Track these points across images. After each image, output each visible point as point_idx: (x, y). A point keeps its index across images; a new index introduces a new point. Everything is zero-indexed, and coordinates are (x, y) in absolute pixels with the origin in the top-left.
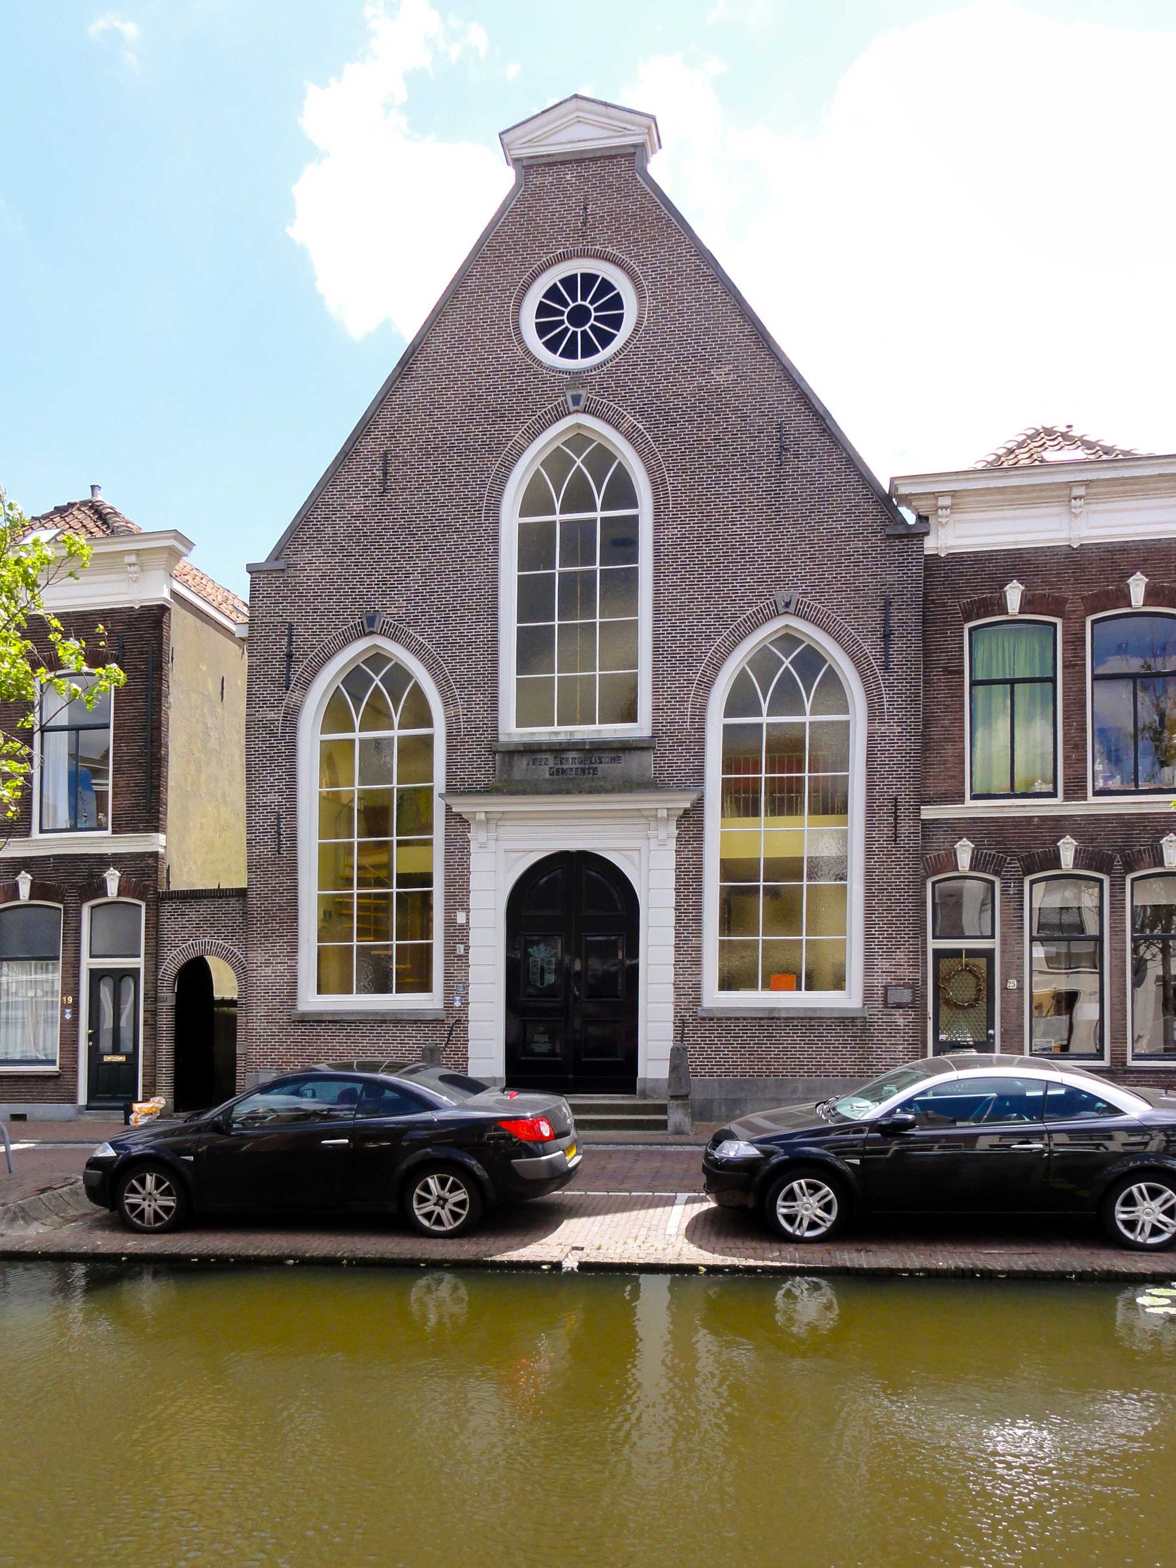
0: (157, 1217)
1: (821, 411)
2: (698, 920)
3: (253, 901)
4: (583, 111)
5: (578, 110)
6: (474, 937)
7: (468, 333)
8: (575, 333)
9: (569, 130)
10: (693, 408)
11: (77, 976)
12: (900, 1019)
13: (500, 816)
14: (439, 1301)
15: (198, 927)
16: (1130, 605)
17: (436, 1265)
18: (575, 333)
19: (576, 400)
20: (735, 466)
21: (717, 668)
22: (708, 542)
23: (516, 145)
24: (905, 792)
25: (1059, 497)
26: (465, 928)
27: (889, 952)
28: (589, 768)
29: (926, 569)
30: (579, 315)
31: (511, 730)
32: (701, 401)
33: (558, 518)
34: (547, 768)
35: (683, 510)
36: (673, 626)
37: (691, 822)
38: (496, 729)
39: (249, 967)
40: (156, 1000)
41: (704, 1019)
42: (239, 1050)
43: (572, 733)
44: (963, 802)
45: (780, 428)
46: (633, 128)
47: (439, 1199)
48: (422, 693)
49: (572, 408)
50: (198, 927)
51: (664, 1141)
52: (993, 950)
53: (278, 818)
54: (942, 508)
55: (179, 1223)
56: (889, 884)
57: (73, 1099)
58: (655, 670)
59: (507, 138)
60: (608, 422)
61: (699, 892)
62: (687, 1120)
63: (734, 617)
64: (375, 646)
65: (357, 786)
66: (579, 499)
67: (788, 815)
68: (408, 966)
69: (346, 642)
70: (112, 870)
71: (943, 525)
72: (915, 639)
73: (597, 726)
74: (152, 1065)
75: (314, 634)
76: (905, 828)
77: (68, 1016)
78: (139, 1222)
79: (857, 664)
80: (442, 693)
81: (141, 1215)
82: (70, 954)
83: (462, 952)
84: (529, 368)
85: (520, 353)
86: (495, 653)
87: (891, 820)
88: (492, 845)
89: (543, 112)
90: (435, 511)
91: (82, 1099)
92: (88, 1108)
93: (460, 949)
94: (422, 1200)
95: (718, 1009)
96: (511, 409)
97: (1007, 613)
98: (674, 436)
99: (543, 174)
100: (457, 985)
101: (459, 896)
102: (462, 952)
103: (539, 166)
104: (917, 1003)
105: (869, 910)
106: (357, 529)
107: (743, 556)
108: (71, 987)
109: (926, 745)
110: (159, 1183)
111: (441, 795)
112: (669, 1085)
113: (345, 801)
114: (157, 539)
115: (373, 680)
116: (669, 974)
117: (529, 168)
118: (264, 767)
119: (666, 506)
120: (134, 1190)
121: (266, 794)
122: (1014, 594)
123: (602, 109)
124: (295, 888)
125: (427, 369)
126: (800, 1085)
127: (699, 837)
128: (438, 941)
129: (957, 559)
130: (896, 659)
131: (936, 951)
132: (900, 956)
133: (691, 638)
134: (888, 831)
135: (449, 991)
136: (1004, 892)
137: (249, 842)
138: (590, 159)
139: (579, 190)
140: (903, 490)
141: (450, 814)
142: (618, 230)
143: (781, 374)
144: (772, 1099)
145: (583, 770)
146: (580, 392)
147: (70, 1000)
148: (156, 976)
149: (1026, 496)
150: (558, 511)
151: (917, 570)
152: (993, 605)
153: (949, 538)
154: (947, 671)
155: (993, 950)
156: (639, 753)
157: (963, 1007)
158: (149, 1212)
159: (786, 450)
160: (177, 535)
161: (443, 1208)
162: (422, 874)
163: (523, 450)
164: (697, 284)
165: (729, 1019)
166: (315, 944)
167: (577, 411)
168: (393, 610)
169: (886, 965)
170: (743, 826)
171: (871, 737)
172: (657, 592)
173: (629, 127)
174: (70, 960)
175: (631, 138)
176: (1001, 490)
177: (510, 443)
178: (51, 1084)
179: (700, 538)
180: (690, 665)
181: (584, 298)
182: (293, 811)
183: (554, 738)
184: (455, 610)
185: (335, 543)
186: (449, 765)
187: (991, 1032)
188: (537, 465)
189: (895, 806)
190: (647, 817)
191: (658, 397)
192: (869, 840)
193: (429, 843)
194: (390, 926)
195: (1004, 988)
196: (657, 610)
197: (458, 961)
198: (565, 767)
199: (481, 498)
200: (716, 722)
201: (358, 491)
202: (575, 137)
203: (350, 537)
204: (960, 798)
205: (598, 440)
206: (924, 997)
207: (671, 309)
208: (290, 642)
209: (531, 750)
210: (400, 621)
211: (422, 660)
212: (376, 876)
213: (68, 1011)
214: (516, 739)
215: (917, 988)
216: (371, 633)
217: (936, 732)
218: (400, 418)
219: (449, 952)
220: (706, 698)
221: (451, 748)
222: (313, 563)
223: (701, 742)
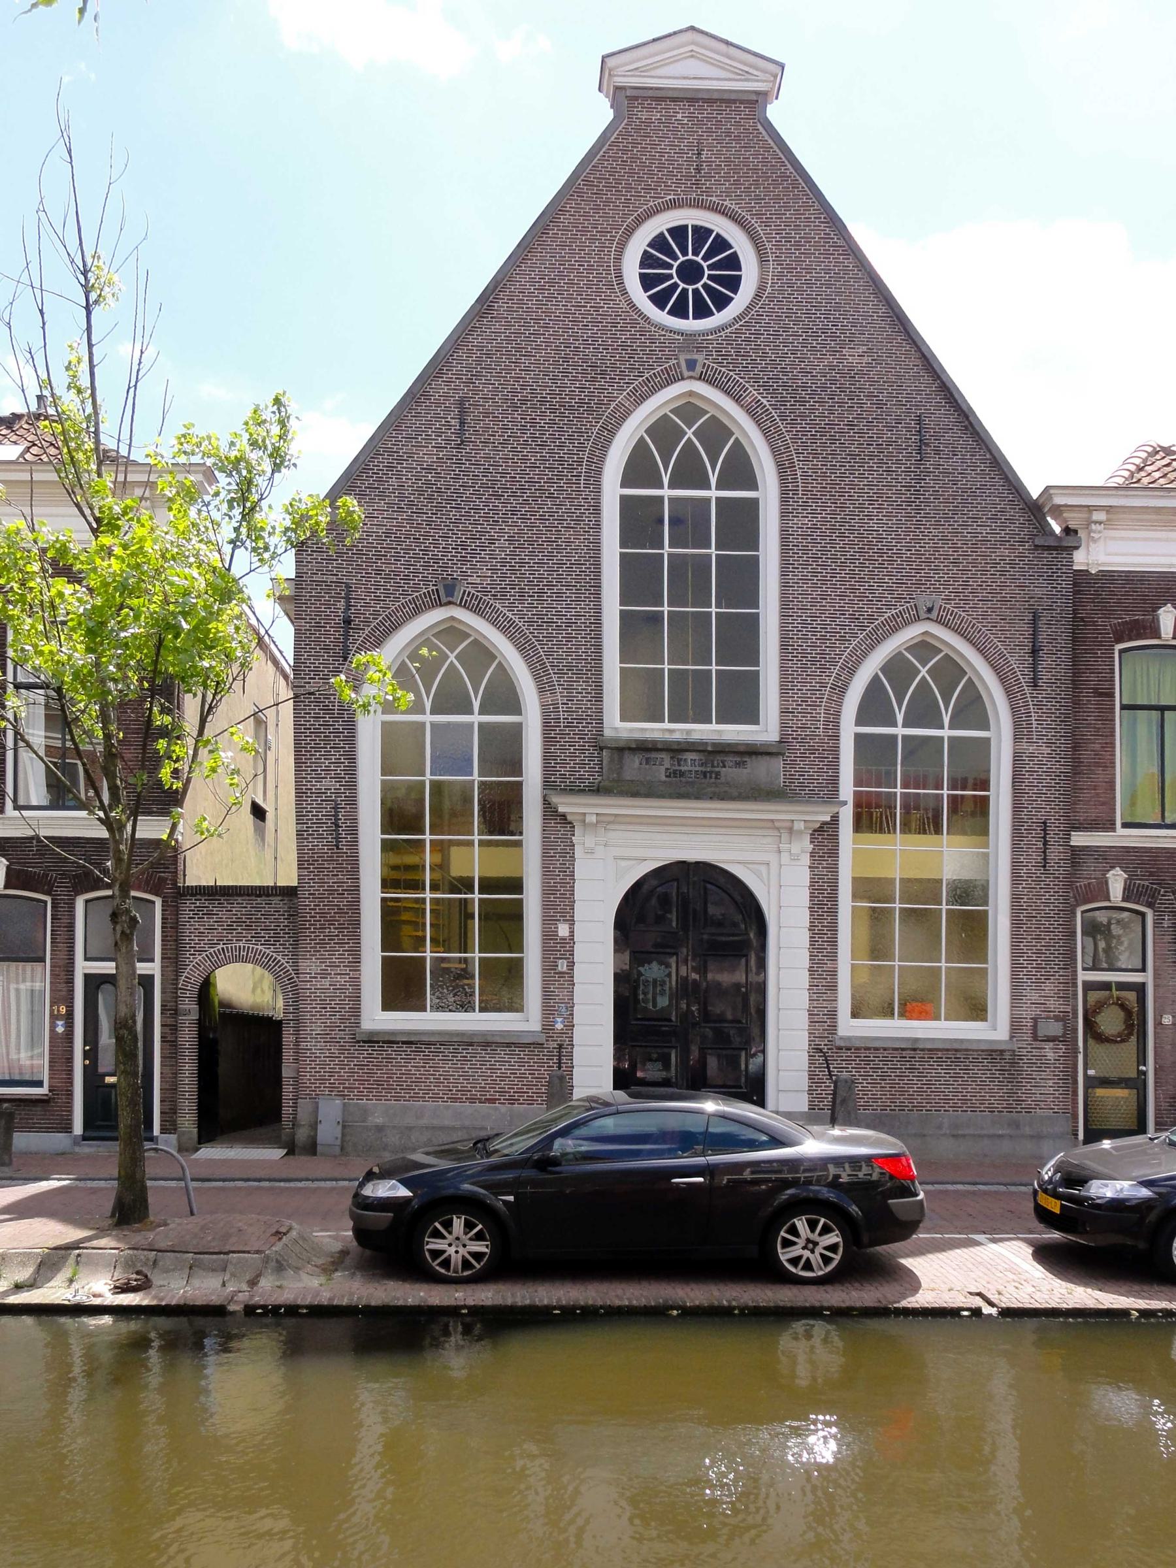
0: (466, 1264)
2: (834, 942)
3: (306, 901)
4: (697, 44)
5: (693, 43)
6: (580, 952)
9: (676, 64)
11: (70, 981)
14: (809, 1352)
16: (1159, 637)
17: (813, 1313)
19: (691, 365)
20: (871, 456)
22: (842, 536)
23: (620, 71)
24: (1054, 815)
27: (1038, 982)
28: (711, 772)
29: (1075, 584)
30: (692, 273)
31: (617, 725)
34: (663, 769)
35: (815, 499)
36: (804, 622)
37: (825, 835)
40: (176, 1012)
41: (840, 1048)
42: (287, 1072)
43: (688, 732)
44: (1114, 829)
45: (919, 420)
46: (756, 73)
47: (809, 1244)
49: (686, 374)
50: (230, 929)
54: (1096, 522)
55: (495, 1270)
57: (67, 1128)
58: (783, 669)
61: (833, 912)
63: (871, 619)
64: (452, 618)
69: (418, 611)
71: (1095, 541)
72: (1065, 655)
74: (171, 1091)
75: (377, 599)
76: (1056, 853)
77: (60, 1030)
78: (443, 1271)
79: (1003, 680)
80: (537, 678)
81: (446, 1263)
82: (63, 955)
83: (565, 969)
84: (634, 323)
85: (623, 304)
86: (599, 637)
89: (654, 40)
90: (523, 473)
91: (78, 1128)
92: (84, 1138)
93: (562, 966)
94: (787, 1244)
98: (803, 416)
99: (650, 109)
101: (560, 902)
102: (565, 969)
103: (645, 98)
104: (1068, 1038)
106: (428, 483)
108: (63, 995)
109: (1076, 769)
110: (469, 1226)
117: (630, 101)
118: (317, 748)
120: (437, 1234)
121: (319, 779)
123: (723, 47)
124: (356, 889)
125: (510, 310)
126: (945, 1120)
127: (834, 853)
129: (1108, 577)
130: (1045, 677)
131: (1085, 983)
132: (1049, 987)
133: (823, 638)
134: (1037, 857)
135: (548, 1010)
136: (1157, 924)
137: (299, 834)
138: (705, 100)
140: (1058, 500)
141: (550, 811)
142: (737, 183)
143: (918, 362)
144: (915, 1135)
145: (705, 774)
146: (695, 357)
147: (63, 1010)
148: (177, 984)
151: (1066, 585)
152: (1145, 628)
154: (1098, 693)
156: (768, 758)
157: (1116, 1042)
158: (456, 1260)
159: (927, 445)
161: (812, 1252)
162: (509, 879)
163: (628, 413)
164: (827, 254)
165: (869, 1049)
167: (691, 377)
168: (476, 578)
169: (1035, 996)
170: (874, 842)
171: (1017, 758)
173: (751, 71)
174: (61, 963)
175: (756, 84)
176: (1158, 510)
177: (613, 405)
178: (38, 1109)
180: (823, 668)
181: (705, 259)
182: (353, 801)
183: (667, 736)
184: (550, 585)
187: (1142, 1068)
188: (642, 432)
189: (1045, 830)
190: (778, 829)
191: (785, 373)
192: (1016, 865)
194: (462, 935)
195: (1158, 1024)
196: (785, 604)
197: (559, 977)
198: (683, 769)
199: (580, 463)
200: (849, 729)
201: (428, 439)
202: (692, 73)
204: (1110, 826)
205: (712, 411)
206: (1075, 1030)
207: (799, 276)
208: (348, 606)
209: (645, 748)
211: (511, 638)
213: (60, 1023)
214: (624, 735)
215: (1066, 1019)
216: (450, 603)
217: (1086, 755)
218: (479, 361)
221: (548, 740)
223: (835, 750)
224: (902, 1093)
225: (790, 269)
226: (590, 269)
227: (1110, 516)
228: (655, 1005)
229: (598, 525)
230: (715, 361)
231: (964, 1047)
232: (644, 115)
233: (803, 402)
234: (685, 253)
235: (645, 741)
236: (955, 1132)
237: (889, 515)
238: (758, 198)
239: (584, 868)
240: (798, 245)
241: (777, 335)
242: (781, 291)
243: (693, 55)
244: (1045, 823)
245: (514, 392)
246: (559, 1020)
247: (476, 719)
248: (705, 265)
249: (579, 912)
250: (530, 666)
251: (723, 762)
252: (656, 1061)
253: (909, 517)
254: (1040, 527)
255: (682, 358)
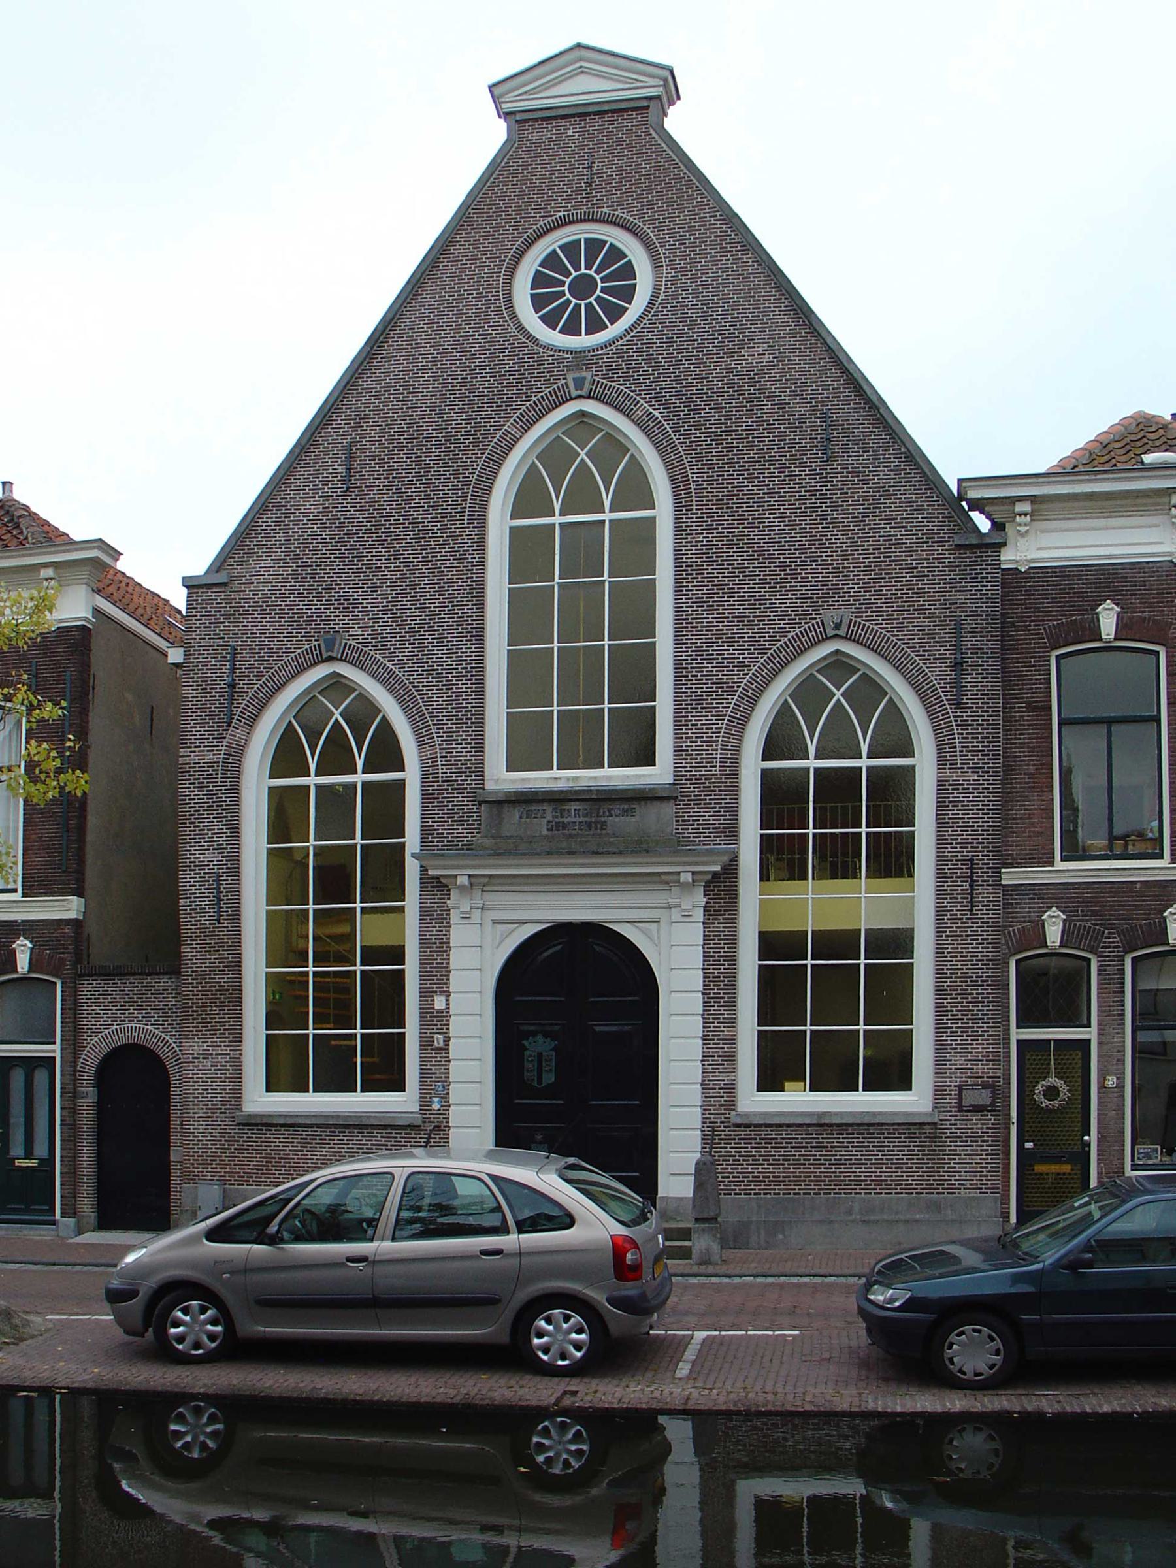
1: (874, 399)
2: (732, 1006)
5: (581, 60)
7: (450, 307)
8: (578, 306)
10: (720, 393)
12: (976, 1123)
13: (486, 880)
15: (123, 1009)
18: (578, 306)
20: (772, 462)
21: (753, 702)
22: (740, 551)
25: (1158, 504)
26: (445, 1014)
28: (596, 823)
31: (500, 777)
32: (731, 385)
33: (557, 519)
34: (544, 821)
35: (710, 513)
37: (721, 888)
38: (481, 774)
39: (183, 1058)
43: (576, 778)
48: (570, 923)
51: (687, 1271)
52: (1089, 1041)
53: (218, 880)
56: (964, 962)
58: (677, 702)
59: (497, 92)
60: (617, 409)
61: (732, 973)
62: (715, 1247)
63: (773, 640)
65: (312, 842)
66: (583, 496)
67: (843, 878)
68: (376, 1059)
70: (22, 941)
71: (1023, 535)
73: (606, 771)
75: (262, 660)
76: (984, 895)
80: (416, 731)
84: (523, 346)
85: (512, 329)
86: (481, 682)
87: (967, 885)
88: (476, 916)
93: (439, 1040)
95: (755, 1114)
96: (501, 394)
97: (1101, 640)
98: (697, 426)
100: (435, 1084)
101: (436, 975)
102: (442, 1044)
103: (536, 120)
105: (940, 993)
106: (314, 535)
107: (783, 567)
109: (1007, 796)
111: (413, 855)
112: (694, 1206)
113: (298, 857)
114: (82, 549)
115: (333, 714)
116: (695, 1071)
118: (201, 819)
119: (689, 507)
122: (1108, 619)
127: (732, 907)
128: (412, 1030)
129: (1040, 574)
130: (970, 691)
132: (978, 1049)
133: (720, 666)
135: (426, 1091)
139: (582, 147)
140: (972, 494)
144: (821, 1222)
145: (589, 825)
146: (584, 374)
148: (75, 1067)
149: (1118, 502)
150: (557, 512)
151: (992, 587)
153: (1033, 548)
154: (1030, 707)
155: (1089, 1041)
156: (657, 804)
160: (100, 544)
164: (724, 253)
166: (263, 1032)
170: (788, 892)
171: (941, 785)
172: (678, 610)
175: (644, 90)
176: (1091, 496)
177: (500, 433)
179: (730, 544)
180: (720, 698)
181: (569, 302)
182: (235, 873)
184: (432, 630)
185: (287, 552)
186: (423, 818)
187: (1086, 1138)
190: (667, 883)
192: (940, 909)
193: (401, 910)
195: (1102, 1087)
197: (436, 1054)
198: (566, 820)
199: (464, 497)
201: (315, 489)
203: (306, 544)
205: (607, 429)
208: (233, 669)
209: (526, 800)
210: (365, 643)
211: (391, 691)
212: (335, 948)
215: (996, 1088)
217: (1019, 779)
219: (426, 1044)
220: (740, 739)
221: (426, 798)
222: (258, 578)
223: (734, 790)
224: (808, 1174)
225: (684, 272)
226: (478, 298)
227: (1036, 507)
228: (540, 1082)
229: (482, 562)
230: (605, 376)
231: (876, 1121)
232: (535, 136)
233: (697, 410)
234: (578, 268)
235: (522, 793)
236: (866, 1218)
237: (792, 525)
238: (651, 205)
239: (459, 935)
240: (693, 246)
241: (670, 341)
242: (674, 297)
243: (582, 71)
244: (971, 860)
245: (401, 432)
246: (436, 1099)
247: (359, 778)
248: (598, 278)
249: (454, 982)
250: (410, 718)
251: (609, 811)
252: (540, 1143)
253: (814, 524)
254: (959, 522)
255: (570, 377)
